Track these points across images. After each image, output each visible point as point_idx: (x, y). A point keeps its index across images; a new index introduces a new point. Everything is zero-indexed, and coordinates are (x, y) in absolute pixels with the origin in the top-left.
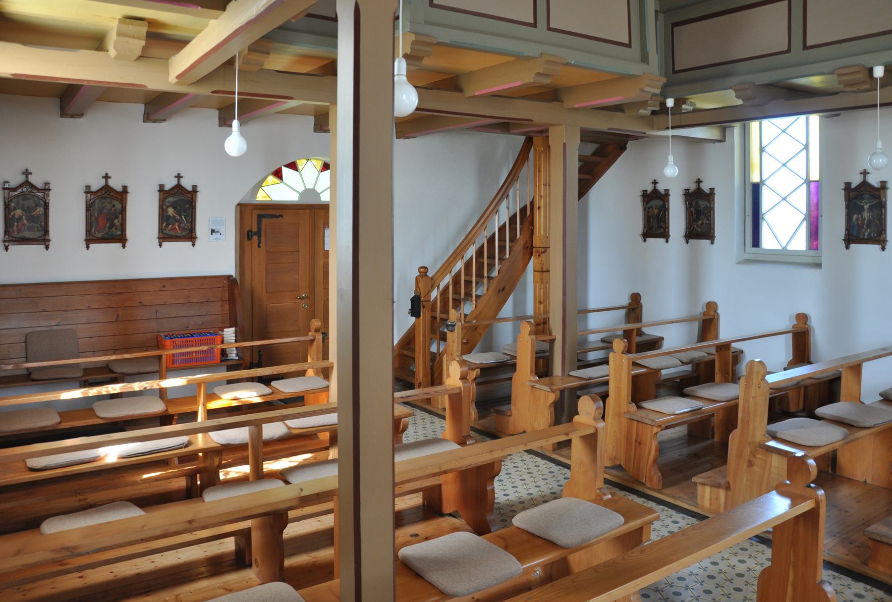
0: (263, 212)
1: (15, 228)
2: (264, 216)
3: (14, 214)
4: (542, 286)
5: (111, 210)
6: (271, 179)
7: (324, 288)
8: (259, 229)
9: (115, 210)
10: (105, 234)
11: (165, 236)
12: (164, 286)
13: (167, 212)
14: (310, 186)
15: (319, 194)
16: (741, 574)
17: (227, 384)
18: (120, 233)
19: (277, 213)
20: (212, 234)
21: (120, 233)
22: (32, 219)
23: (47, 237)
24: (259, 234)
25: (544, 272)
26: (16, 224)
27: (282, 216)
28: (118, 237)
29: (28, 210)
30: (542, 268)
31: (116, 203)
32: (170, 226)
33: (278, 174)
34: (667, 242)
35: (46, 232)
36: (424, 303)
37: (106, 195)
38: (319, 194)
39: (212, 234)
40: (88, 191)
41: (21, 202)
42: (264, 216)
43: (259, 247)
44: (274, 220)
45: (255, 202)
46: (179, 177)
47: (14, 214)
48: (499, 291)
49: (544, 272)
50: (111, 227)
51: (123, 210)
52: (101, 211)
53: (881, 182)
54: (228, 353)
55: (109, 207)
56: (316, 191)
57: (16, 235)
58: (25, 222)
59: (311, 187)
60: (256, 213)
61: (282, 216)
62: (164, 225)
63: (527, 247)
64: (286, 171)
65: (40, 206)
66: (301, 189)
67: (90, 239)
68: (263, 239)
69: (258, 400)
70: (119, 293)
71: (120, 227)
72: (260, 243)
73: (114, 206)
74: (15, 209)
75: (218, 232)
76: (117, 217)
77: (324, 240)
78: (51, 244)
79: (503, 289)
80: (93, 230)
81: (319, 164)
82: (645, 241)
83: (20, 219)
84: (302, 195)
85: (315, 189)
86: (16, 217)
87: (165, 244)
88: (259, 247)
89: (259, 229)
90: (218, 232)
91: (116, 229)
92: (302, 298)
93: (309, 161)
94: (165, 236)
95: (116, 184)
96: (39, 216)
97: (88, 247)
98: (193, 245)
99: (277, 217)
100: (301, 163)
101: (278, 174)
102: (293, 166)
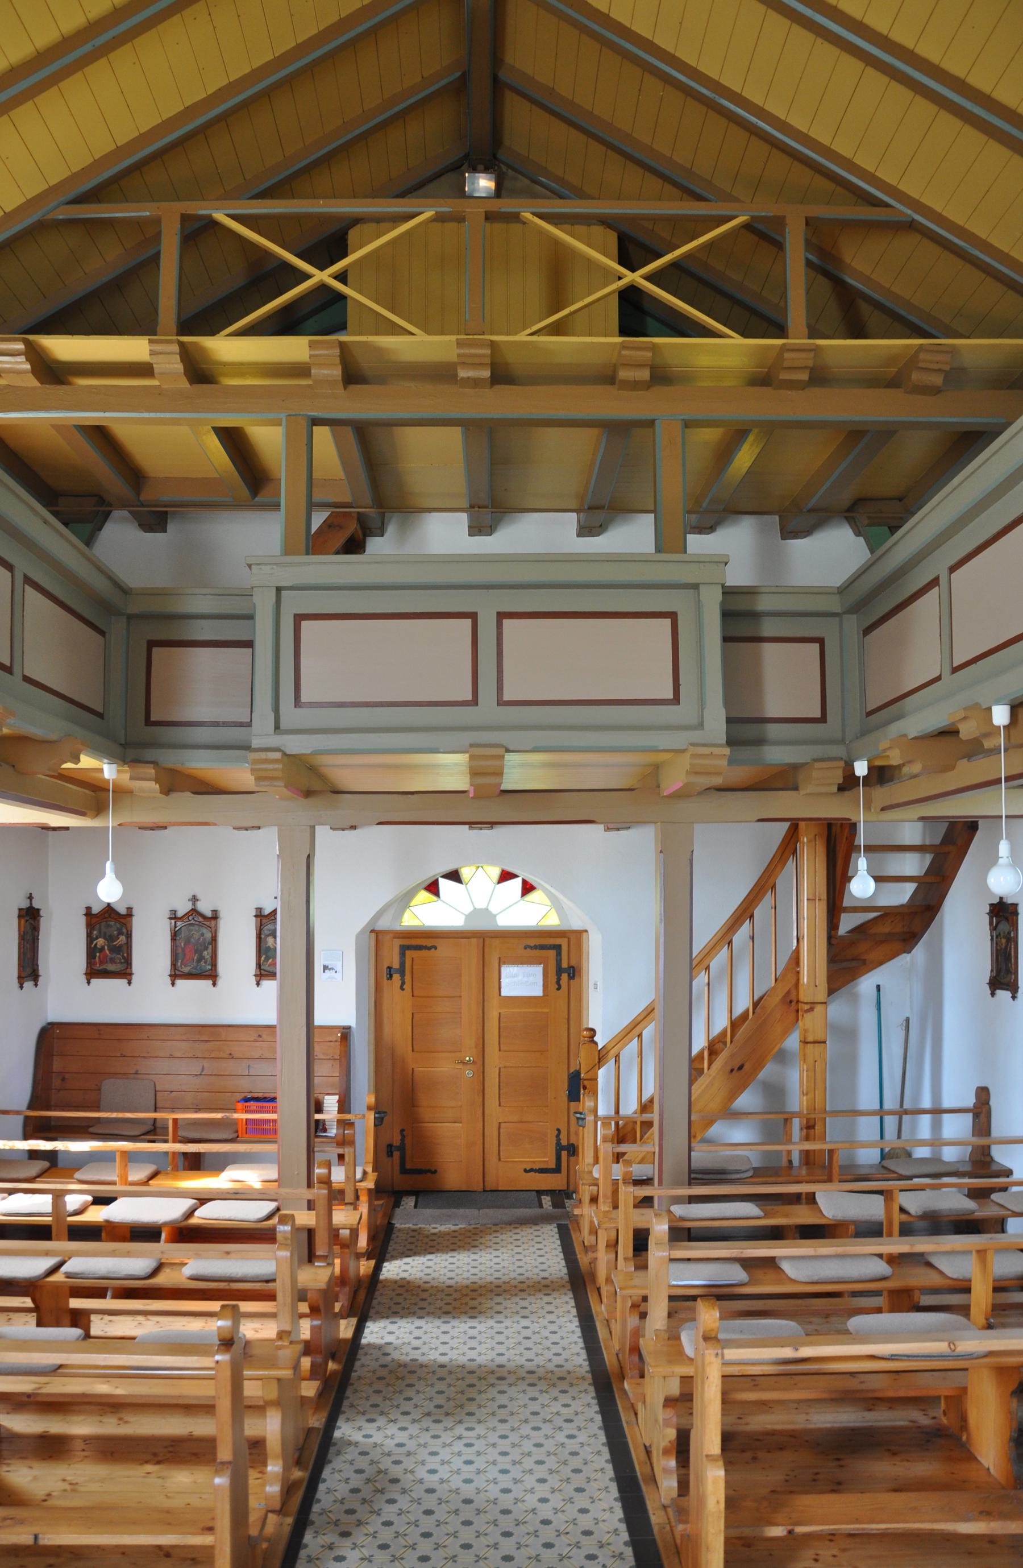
0: (406, 942)
1: (97, 958)
2: (409, 947)
3: (96, 944)
4: (805, 1067)
5: (199, 939)
6: (424, 895)
7: (500, 1050)
8: (403, 964)
9: (204, 940)
10: (193, 968)
11: (94, 971)
12: (260, 1036)
13: (267, 942)
14: (481, 905)
15: (495, 916)
16: (549, 1543)
17: (690, 1203)
18: (210, 967)
19: (429, 943)
20: (324, 972)
21: (210, 967)
22: (112, 949)
23: (128, 971)
24: (402, 971)
25: (807, 1043)
26: (98, 954)
27: (436, 948)
28: (207, 973)
29: (110, 939)
30: (805, 1038)
31: (204, 931)
32: (270, 961)
33: (433, 888)
34: (1014, 1000)
35: (128, 962)
36: (586, 1083)
37: (192, 922)
38: (495, 916)
39: (324, 972)
40: (174, 917)
41: (103, 930)
42: (409, 947)
43: (402, 989)
44: (424, 953)
45: (398, 928)
46: (194, 899)
47: (96, 944)
48: (732, 1071)
49: (807, 1043)
50: (199, 961)
51: (214, 939)
52: (188, 941)
53: (128, 908)
54: (327, 1127)
55: (197, 935)
56: (481, 910)
57: (98, 967)
58: (107, 952)
59: (483, 906)
60: (397, 943)
61: (436, 948)
62: (263, 958)
63: (791, 1002)
64: (444, 884)
65: (122, 934)
66: (468, 909)
67: (176, 975)
68: (408, 978)
69: (258, 1185)
70: (207, 1041)
71: (209, 960)
72: (403, 983)
73: (203, 935)
74: (97, 938)
75: (332, 969)
76: (206, 949)
77: (500, 983)
78: (134, 978)
79: (740, 1068)
80: (179, 964)
81: (496, 872)
82: (993, 994)
83: (102, 949)
84: (468, 917)
85: (489, 909)
86: (98, 946)
87: (93, 981)
88: (402, 989)
89: (403, 964)
90: (332, 969)
91: (205, 962)
92: (463, 1063)
93: (480, 868)
94: (94, 971)
95: (205, 907)
96: (121, 946)
97: (173, 984)
98: (129, 983)
99: (429, 948)
100: (465, 873)
101: (433, 888)
102: (454, 876)
